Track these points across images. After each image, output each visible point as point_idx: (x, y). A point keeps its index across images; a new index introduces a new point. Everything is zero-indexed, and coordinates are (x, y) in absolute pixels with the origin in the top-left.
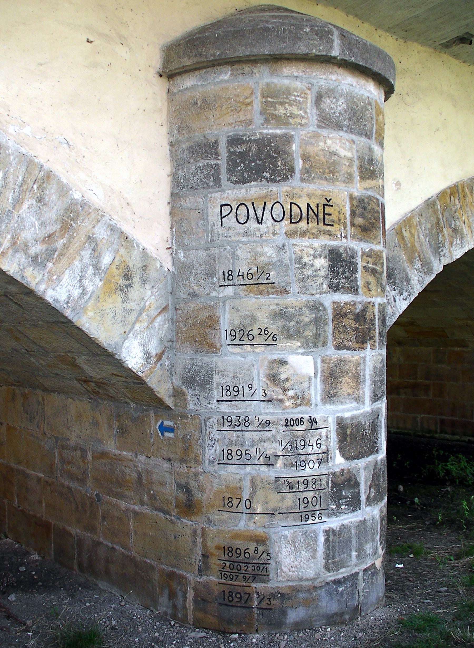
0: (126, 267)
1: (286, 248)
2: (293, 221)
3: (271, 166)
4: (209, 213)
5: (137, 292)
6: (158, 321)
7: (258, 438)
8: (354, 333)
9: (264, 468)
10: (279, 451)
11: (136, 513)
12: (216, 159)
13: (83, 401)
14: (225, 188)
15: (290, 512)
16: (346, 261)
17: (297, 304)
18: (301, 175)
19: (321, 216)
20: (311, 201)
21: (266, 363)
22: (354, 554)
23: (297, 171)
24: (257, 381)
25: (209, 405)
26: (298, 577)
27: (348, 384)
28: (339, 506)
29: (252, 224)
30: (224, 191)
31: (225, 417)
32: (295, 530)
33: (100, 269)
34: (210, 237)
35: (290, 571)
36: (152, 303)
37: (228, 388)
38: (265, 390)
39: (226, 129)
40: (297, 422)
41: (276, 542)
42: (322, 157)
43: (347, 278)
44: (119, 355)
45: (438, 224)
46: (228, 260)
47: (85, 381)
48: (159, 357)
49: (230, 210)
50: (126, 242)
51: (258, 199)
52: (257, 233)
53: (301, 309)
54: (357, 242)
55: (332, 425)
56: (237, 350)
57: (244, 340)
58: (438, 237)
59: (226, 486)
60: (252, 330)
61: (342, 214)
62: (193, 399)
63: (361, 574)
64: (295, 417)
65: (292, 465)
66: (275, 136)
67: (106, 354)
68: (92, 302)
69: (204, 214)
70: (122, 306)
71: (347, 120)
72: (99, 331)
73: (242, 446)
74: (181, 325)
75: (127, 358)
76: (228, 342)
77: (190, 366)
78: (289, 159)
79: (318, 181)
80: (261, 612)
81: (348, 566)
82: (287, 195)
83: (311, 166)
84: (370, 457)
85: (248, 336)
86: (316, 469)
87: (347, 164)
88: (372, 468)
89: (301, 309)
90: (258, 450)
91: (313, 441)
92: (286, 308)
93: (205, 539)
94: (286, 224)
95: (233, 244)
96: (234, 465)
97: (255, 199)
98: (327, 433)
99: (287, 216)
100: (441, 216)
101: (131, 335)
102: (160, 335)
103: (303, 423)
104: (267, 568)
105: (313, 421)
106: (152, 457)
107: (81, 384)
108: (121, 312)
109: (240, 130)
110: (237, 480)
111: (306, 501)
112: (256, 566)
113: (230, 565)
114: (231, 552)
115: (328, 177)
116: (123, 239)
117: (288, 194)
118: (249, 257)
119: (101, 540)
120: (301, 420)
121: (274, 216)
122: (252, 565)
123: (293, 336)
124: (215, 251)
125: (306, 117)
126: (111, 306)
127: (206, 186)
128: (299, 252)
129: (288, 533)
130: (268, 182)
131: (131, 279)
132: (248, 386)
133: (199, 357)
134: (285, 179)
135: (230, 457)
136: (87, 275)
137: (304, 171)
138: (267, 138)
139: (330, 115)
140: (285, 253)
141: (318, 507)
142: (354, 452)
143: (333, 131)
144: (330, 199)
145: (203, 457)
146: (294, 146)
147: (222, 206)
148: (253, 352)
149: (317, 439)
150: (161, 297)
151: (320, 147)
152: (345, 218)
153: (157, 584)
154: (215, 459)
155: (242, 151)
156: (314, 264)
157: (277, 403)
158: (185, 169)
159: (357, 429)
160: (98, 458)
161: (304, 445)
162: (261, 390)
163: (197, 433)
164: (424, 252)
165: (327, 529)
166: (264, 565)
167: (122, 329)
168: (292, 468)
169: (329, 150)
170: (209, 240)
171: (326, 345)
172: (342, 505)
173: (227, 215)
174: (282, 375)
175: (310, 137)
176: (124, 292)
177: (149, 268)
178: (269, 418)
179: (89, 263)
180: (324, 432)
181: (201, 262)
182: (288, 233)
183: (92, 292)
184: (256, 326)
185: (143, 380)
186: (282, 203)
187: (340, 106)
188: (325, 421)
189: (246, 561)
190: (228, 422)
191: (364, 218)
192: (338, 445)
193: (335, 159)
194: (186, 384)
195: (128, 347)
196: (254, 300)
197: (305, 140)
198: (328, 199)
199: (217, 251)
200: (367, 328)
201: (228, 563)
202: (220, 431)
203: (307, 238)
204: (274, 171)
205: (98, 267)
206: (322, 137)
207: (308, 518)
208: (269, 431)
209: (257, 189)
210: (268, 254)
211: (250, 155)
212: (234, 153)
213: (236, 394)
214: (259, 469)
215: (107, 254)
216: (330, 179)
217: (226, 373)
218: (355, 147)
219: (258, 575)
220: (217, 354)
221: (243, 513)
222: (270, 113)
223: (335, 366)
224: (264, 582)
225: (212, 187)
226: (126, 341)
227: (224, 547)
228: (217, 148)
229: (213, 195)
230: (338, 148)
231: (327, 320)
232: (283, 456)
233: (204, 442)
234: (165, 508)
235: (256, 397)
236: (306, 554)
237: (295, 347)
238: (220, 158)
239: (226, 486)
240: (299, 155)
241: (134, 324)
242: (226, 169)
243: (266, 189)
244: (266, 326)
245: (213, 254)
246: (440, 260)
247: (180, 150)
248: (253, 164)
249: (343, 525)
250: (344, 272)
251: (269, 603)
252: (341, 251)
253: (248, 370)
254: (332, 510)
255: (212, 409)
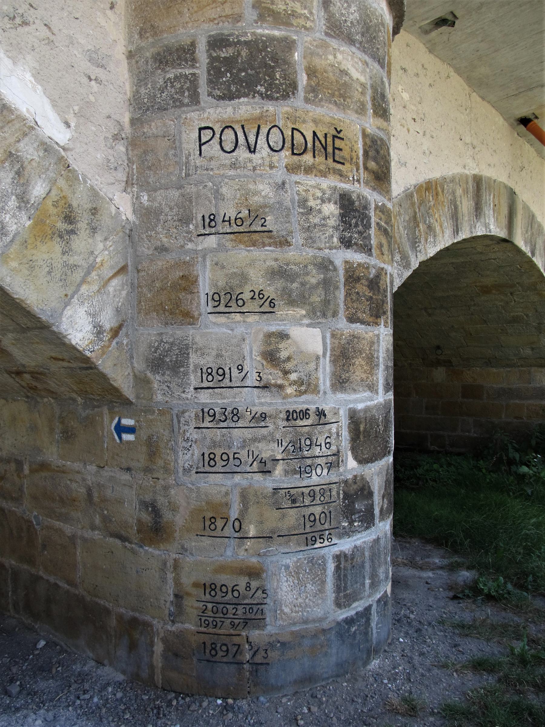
0: (67, 205)
1: (287, 186)
2: (295, 152)
3: (267, 78)
4: (183, 139)
5: (84, 242)
6: (113, 284)
7: (250, 436)
8: (368, 303)
9: (258, 477)
10: (278, 453)
11: (85, 540)
12: (193, 66)
13: (18, 400)
14: (205, 105)
15: (293, 533)
16: (359, 212)
17: (300, 260)
18: (306, 93)
19: (330, 149)
20: (318, 129)
21: (261, 336)
22: (368, 581)
23: (300, 88)
24: (249, 360)
25: (183, 395)
26: (303, 619)
27: (362, 368)
28: (351, 523)
29: (242, 153)
30: (203, 109)
31: (206, 410)
32: (299, 557)
33: (29, 203)
34: (184, 171)
35: (292, 612)
36: (106, 260)
37: (209, 371)
38: (260, 373)
39: (206, 26)
40: (301, 414)
41: (275, 575)
42: (331, 74)
43: (360, 233)
44: (58, 327)
45: (415, 217)
46: (209, 201)
47: (19, 373)
48: (116, 332)
49: (212, 135)
50: (67, 171)
51: (249, 120)
52: (248, 164)
53: (306, 266)
54: (371, 191)
55: (343, 418)
56: (222, 319)
57: (231, 307)
58: (415, 231)
59: (208, 503)
60: (242, 293)
61: (354, 151)
62: (161, 387)
63: (374, 607)
64: (300, 407)
65: (295, 472)
66: (272, 39)
67: (39, 325)
68: (15, 246)
69: (177, 142)
70: (61, 258)
71: (360, 35)
72: (27, 290)
73: (230, 448)
74: (145, 290)
75: (70, 331)
76: (210, 309)
77: (156, 344)
78: (290, 71)
79: (327, 105)
80: (254, 669)
81: (361, 599)
82: (288, 118)
83: (318, 84)
84: (383, 460)
85: (237, 300)
86: (324, 476)
87: (360, 90)
88: (384, 473)
89: (306, 266)
90: (251, 453)
91: (321, 440)
92: (287, 265)
93: (178, 574)
94: (286, 156)
95: (216, 179)
96: (217, 474)
97: (245, 120)
98: (337, 429)
99: (288, 144)
100: (417, 211)
101: (75, 300)
102: (115, 303)
103: (309, 415)
104: (262, 610)
105: (321, 413)
106: (106, 466)
107: (13, 378)
108: (59, 266)
109: (226, 28)
110: (223, 493)
111: (312, 518)
112: (248, 607)
113: (213, 608)
114: (214, 590)
115: (338, 102)
116: (63, 166)
117: (289, 117)
118: (238, 196)
119: (41, 573)
120: (306, 413)
121: (271, 144)
122: (243, 606)
123: (297, 302)
124: (191, 189)
125: (312, 19)
126: (46, 256)
127: (178, 104)
128: (304, 193)
129: (290, 561)
130: (263, 99)
131: (75, 223)
132: (238, 368)
133: (169, 330)
134: (285, 97)
135: (212, 463)
136: (7, 208)
137: (310, 88)
138: (262, 40)
139: (341, 23)
140: (286, 192)
141: (326, 526)
142: (367, 454)
143: (344, 44)
144: (341, 131)
145: (176, 465)
146: (296, 54)
147: (200, 129)
148: (244, 322)
149: (325, 436)
150: (117, 253)
151: (329, 61)
152: (358, 158)
153: (113, 633)
154: (191, 466)
155: (228, 56)
156: (323, 210)
157: (276, 389)
158: (150, 84)
159: (371, 425)
160: (37, 471)
161: (310, 445)
162: (254, 373)
163: (166, 433)
164: (403, 244)
165: (338, 553)
166: (259, 606)
167: (62, 290)
168: (295, 476)
169: (340, 66)
170: (184, 175)
171: (337, 315)
172: (355, 521)
173: (207, 142)
174: (282, 353)
175: (316, 46)
176: (64, 240)
177: (100, 213)
178: (265, 409)
179: (10, 191)
180: (334, 428)
181: (173, 204)
182: (289, 167)
183: (16, 234)
184: (247, 289)
185: (93, 363)
186: (281, 128)
187: (352, 14)
188: (335, 414)
189: (235, 601)
190: (210, 416)
191: (377, 163)
192: (350, 445)
193: (347, 80)
194: (152, 368)
195: (71, 316)
196: (244, 253)
197: (310, 49)
198: (339, 130)
199: (194, 189)
200: (381, 300)
201: (210, 606)
202: (199, 428)
203: (313, 175)
204: (270, 85)
205: (25, 199)
206: (331, 48)
207: (316, 541)
208: (265, 427)
209: (249, 108)
210: (263, 194)
211: (240, 61)
212: (217, 59)
213: (221, 378)
214: (252, 478)
215: (39, 184)
216: (341, 104)
217: (207, 351)
218: (368, 70)
219: (251, 619)
220: (194, 326)
221: (230, 537)
222: (265, 7)
223: (348, 343)
224: (258, 627)
225: (187, 105)
226: (68, 308)
227: (205, 584)
228: (194, 52)
229: (188, 115)
230: (349, 67)
231: (338, 284)
232: (283, 460)
233: (176, 444)
234: (123, 533)
235: (248, 382)
236: (313, 588)
237: (298, 316)
238: (198, 65)
239: (208, 503)
240: (303, 67)
241: (79, 286)
242: (206, 80)
243: (260, 107)
244: (261, 288)
245: (188, 194)
246: (416, 255)
247: (143, 60)
248: (243, 74)
249: (356, 547)
250: (356, 225)
251: (266, 656)
252: (353, 197)
253: (237, 346)
254: (344, 528)
255: (187, 399)
